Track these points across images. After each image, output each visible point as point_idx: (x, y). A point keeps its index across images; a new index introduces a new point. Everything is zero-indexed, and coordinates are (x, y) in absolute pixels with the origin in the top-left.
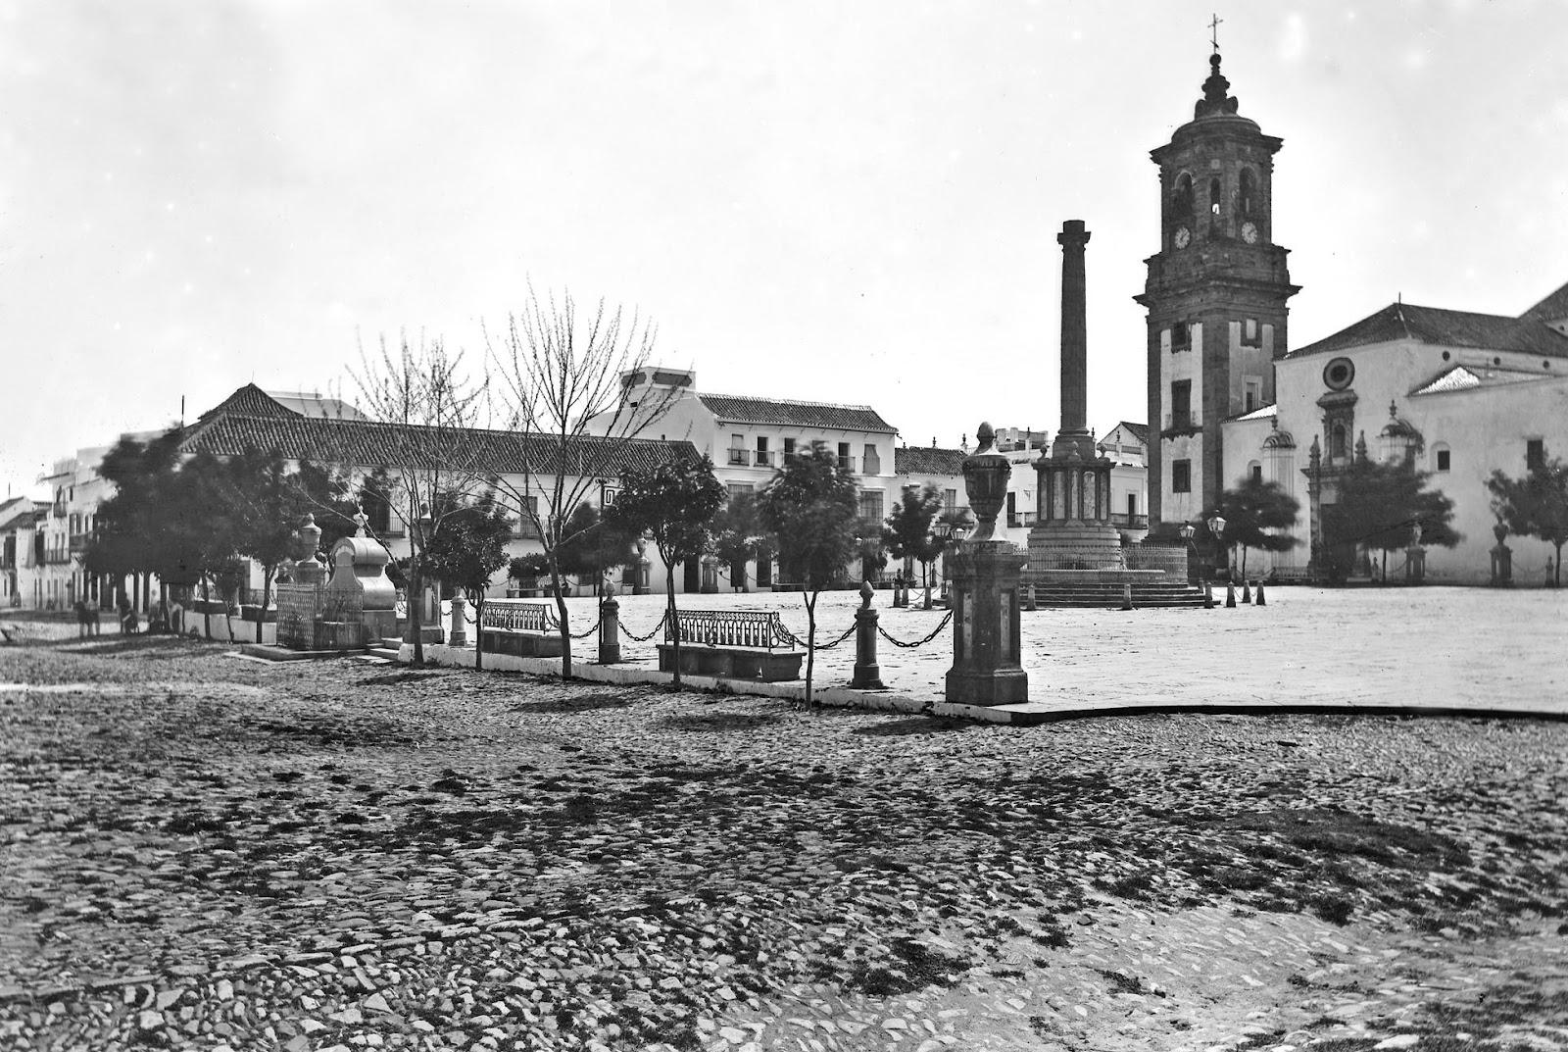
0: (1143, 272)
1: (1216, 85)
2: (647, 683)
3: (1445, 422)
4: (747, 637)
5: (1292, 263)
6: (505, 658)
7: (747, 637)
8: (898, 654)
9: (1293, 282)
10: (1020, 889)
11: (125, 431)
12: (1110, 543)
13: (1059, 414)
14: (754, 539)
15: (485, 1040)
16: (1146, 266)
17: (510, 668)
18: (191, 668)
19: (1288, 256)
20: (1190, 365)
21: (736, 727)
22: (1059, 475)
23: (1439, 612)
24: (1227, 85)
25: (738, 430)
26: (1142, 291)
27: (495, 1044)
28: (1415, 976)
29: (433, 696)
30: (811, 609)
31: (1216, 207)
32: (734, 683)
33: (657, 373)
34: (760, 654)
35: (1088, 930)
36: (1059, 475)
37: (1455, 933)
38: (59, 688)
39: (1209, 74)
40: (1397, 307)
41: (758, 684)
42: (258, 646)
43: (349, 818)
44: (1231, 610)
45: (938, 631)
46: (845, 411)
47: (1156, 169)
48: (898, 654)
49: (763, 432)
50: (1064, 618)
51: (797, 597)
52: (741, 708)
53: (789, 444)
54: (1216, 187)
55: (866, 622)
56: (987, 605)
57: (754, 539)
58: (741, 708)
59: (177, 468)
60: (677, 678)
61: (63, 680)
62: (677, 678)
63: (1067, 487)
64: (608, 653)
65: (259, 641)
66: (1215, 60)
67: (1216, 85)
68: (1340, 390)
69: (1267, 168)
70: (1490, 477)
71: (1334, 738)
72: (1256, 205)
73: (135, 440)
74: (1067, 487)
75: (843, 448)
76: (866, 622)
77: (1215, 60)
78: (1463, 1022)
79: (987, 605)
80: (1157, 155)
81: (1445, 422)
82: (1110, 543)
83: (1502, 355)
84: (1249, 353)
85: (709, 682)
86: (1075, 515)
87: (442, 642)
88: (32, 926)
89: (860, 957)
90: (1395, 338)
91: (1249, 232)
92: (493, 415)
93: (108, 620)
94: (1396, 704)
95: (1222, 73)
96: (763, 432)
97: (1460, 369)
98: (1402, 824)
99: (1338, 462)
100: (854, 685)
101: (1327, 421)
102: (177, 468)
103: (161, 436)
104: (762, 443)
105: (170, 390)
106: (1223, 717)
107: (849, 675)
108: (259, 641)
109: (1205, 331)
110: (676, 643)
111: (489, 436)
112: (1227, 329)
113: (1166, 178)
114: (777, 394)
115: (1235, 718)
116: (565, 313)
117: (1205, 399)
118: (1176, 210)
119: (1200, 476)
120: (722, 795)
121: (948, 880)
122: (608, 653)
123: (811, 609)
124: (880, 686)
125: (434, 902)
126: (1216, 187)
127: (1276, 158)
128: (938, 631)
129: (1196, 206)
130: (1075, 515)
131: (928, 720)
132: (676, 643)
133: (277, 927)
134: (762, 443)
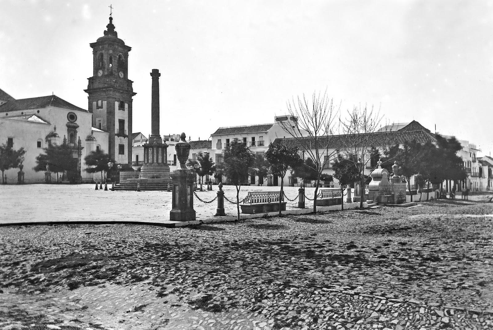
0: (87, 82)
1: (111, 27)
2: (289, 214)
3: (39, 132)
4: (258, 200)
5: (134, 86)
6: (334, 206)
7: (258, 200)
8: (211, 205)
9: (134, 91)
10: (172, 279)
11: (454, 135)
12: (144, 170)
13: (160, 130)
14: (256, 169)
15: (337, 328)
16: (88, 80)
17: (333, 210)
18: (433, 209)
19: (133, 83)
20: (119, 115)
21: (262, 228)
22: (160, 149)
23: (40, 192)
24: (114, 28)
25: (261, 135)
26: (86, 88)
27: (340, 326)
28: (383, 257)
29: (357, 218)
30: (238, 191)
31: (111, 65)
32: (270, 214)
33: (277, 118)
34: (254, 205)
35: (151, 292)
36: (160, 149)
37: (38, 292)
38: (474, 216)
39: (109, 23)
40: (54, 96)
41: (255, 215)
42: (412, 203)
43: (48, 306)
44: (106, 191)
45: (198, 198)
46: (227, 129)
47: (92, 50)
48: (211, 205)
49: (253, 136)
50: (158, 194)
51: (234, 187)
52: (260, 222)
53: (228, 141)
54: (111, 59)
55: (221, 195)
56: (182, 190)
57: (256, 169)
58: (260, 222)
59: (437, 147)
60: (280, 213)
61: (473, 213)
62: (280, 213)
63: (158, 153)
64: (302, 205)
65: (412, 201)
66: (111, 19)
67: (111, 27)
68: (72, 122)
69: (126, 56)
70: (24, 150)
71: (73, 231)
72: (123, 66)
73: (443, 137)
74: (158, 153)
75: (245, 139)
76: (221, 195)
77: (111, 19)
78: (33, 321)
79: (182, 190)
80: (129, 49)
81: (39, 132)
82: (144, 170)
83: (24, 111)
84: (100, 111)
85: (262, 214)
86: (155, 162)
87: (351, 202)
88: (483, 290)
89: (223, 300)
90: (54, 106)
91: (121, 75)
92: (338, 130)
93: (459, 195)
94: (54, 221)
95: (113, 23)
96: (253, 136)
97: (34, 116)
98: (52, 258)
99: (72, 145)
100: (216, 215)
101: (69, 131)
102: (437, 147)
103: (450, 138)
104: (253, 139)
105: (439, 122)
106: (105, 225)
107: (215, 212)
108: (412, 201)
109: (107, 103)
110: (280, 202)
111: (339, 137)
112: (114, 104)
113: (95, 53)
114: (249, 124)
115: (108, 225)
116: (318, 98)
117: (114, 125)
118: (98, 65)
119: (116, 149)
120: (266, 249)
121: (195, 276)
122: (302, 205)
123: (238, 191)
124: (224, 215)
125: (356, 283)
126: (111, 59)
127: (129, 53)
128: (198, 198)
129: (117, 65)
130: (155, 162)
131: (201, 226)
132: (280, 202)
133: (406, 291)
134: (253, 139)
